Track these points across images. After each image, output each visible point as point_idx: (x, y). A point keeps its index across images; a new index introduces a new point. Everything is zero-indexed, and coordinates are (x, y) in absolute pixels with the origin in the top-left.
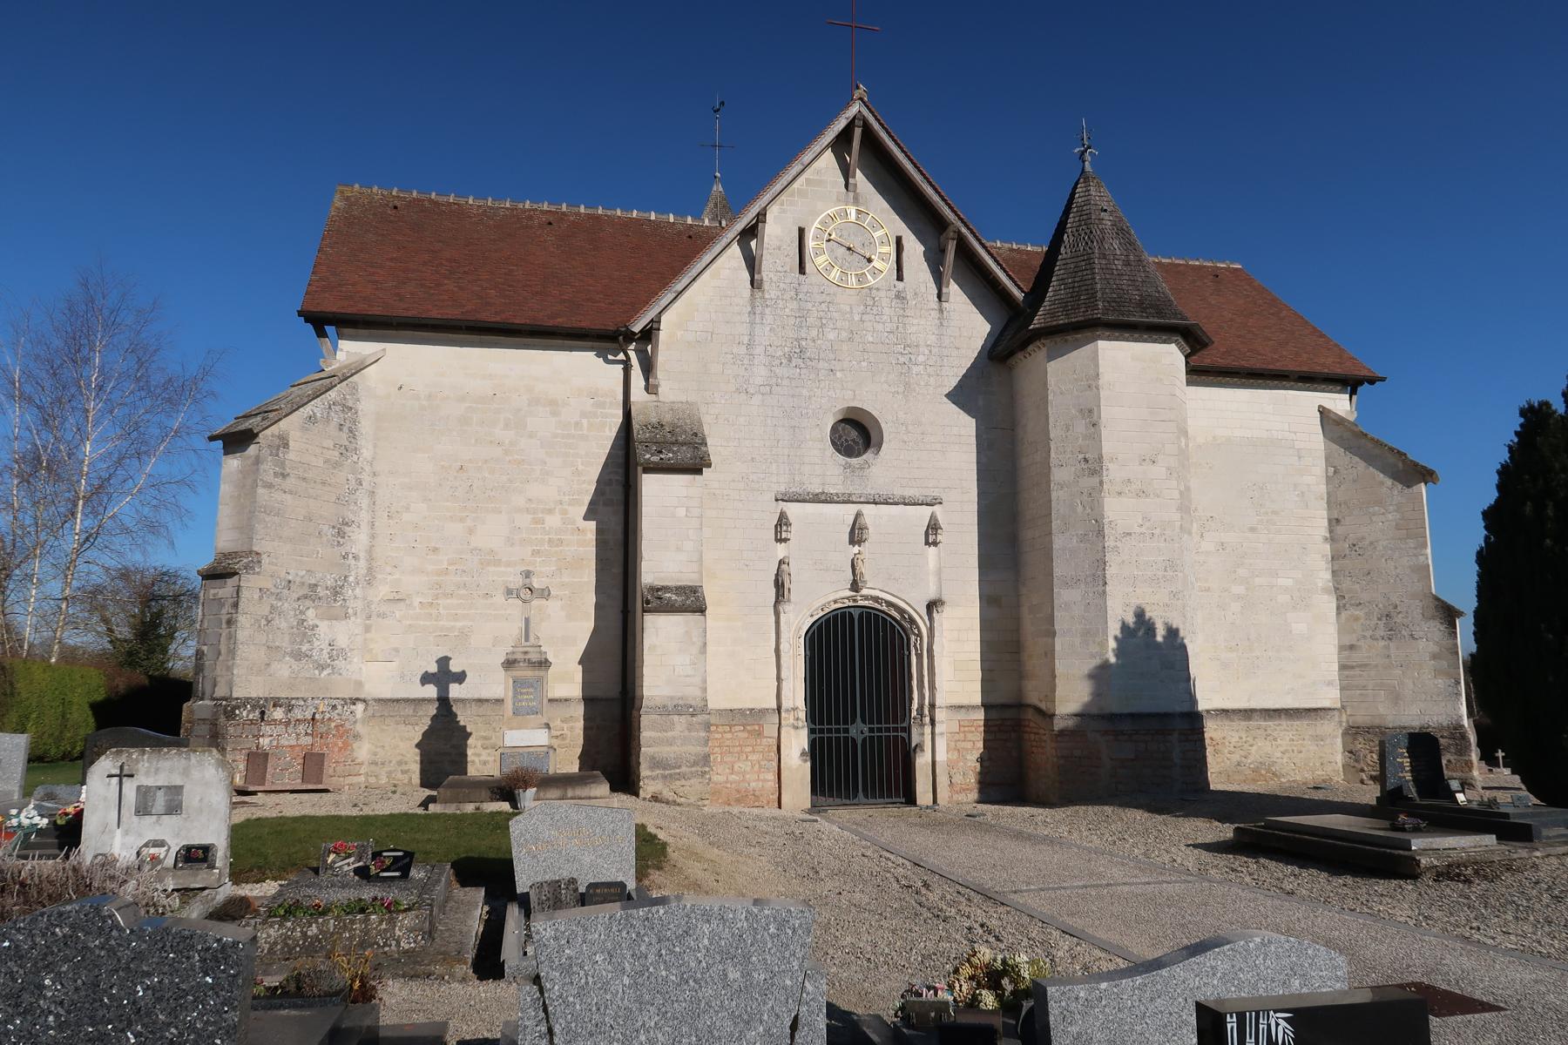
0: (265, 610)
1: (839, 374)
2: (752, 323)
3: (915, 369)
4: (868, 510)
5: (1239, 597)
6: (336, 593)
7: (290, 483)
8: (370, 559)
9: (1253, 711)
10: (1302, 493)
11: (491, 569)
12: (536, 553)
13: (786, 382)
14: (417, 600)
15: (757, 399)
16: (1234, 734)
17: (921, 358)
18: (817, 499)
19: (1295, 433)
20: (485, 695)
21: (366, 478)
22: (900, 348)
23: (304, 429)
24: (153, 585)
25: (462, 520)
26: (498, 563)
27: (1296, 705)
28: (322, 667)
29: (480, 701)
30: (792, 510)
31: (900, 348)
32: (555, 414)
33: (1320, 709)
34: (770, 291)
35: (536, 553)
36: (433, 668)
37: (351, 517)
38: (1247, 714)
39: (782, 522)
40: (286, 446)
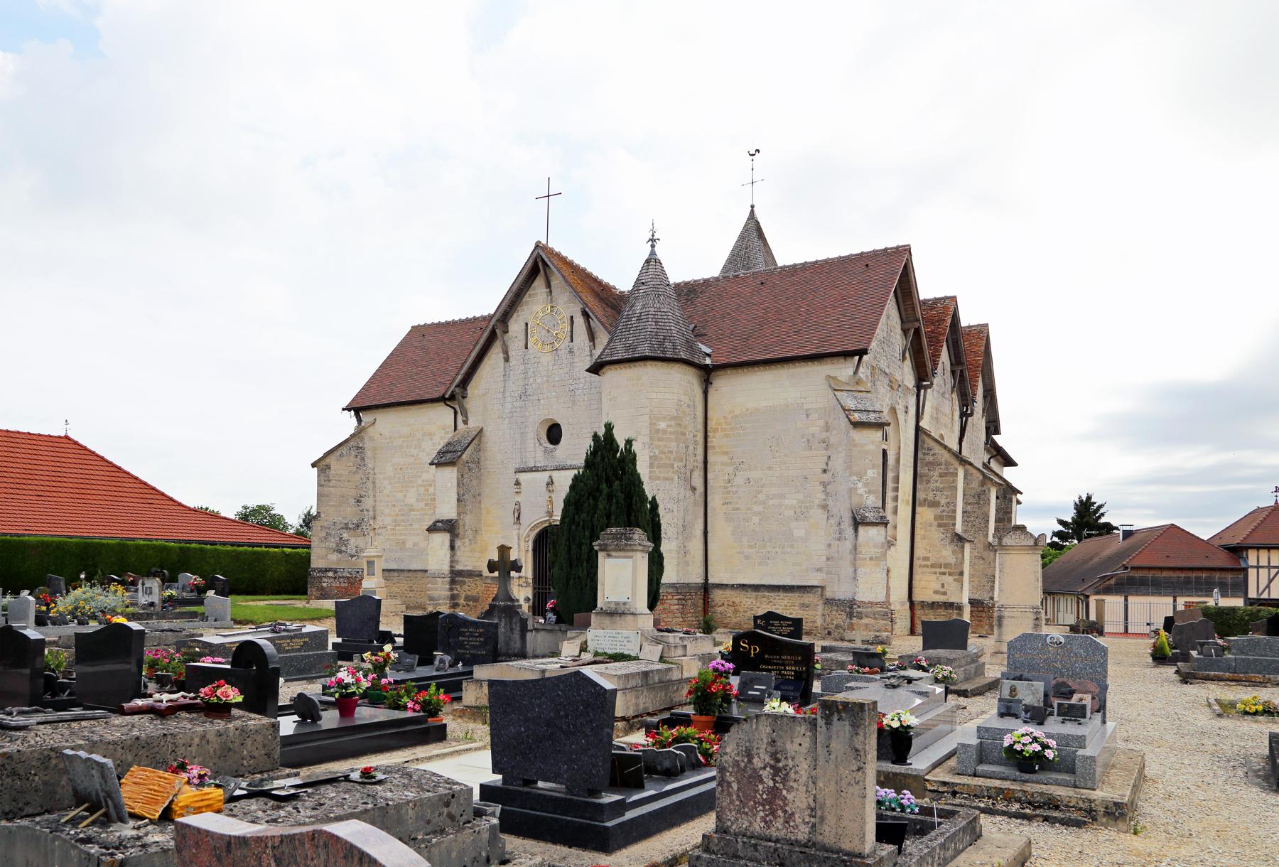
0: (324, 534)
1: (542, 401)
2: (504, 381)
3: (578, 392)
4: (555, 474)
5: (759, 513)
6: (358, 526)
7: (332, 483)
8: (374, 511)
9: (746, 585)
10: (808, 440)
11: (412, 513)
12: (427, 504)
13: (519, 410)
14: (389, 527)
15: (506, 421)
16: (747, 600)
17: (581, 385)
18: (531, 470)
19: (805, 398)
20: (411, 568)
21: (371, 476)
22: (571, 381)
23: (337, 460)
24: (639, 496)
25: (402, 492)
26: (414, 510)
27: (794, 583)
28: (352, 556)
29: (409, 571)
30: (523, 477)
31: (571, 381)
32: (431, 439)
33: (809, 586)
34: (513, 361)
35: (427, 504)
36: (495, 557)
37: (364, 493)
38: (756, 588)
39: (518, 483)
40: (330, 468)
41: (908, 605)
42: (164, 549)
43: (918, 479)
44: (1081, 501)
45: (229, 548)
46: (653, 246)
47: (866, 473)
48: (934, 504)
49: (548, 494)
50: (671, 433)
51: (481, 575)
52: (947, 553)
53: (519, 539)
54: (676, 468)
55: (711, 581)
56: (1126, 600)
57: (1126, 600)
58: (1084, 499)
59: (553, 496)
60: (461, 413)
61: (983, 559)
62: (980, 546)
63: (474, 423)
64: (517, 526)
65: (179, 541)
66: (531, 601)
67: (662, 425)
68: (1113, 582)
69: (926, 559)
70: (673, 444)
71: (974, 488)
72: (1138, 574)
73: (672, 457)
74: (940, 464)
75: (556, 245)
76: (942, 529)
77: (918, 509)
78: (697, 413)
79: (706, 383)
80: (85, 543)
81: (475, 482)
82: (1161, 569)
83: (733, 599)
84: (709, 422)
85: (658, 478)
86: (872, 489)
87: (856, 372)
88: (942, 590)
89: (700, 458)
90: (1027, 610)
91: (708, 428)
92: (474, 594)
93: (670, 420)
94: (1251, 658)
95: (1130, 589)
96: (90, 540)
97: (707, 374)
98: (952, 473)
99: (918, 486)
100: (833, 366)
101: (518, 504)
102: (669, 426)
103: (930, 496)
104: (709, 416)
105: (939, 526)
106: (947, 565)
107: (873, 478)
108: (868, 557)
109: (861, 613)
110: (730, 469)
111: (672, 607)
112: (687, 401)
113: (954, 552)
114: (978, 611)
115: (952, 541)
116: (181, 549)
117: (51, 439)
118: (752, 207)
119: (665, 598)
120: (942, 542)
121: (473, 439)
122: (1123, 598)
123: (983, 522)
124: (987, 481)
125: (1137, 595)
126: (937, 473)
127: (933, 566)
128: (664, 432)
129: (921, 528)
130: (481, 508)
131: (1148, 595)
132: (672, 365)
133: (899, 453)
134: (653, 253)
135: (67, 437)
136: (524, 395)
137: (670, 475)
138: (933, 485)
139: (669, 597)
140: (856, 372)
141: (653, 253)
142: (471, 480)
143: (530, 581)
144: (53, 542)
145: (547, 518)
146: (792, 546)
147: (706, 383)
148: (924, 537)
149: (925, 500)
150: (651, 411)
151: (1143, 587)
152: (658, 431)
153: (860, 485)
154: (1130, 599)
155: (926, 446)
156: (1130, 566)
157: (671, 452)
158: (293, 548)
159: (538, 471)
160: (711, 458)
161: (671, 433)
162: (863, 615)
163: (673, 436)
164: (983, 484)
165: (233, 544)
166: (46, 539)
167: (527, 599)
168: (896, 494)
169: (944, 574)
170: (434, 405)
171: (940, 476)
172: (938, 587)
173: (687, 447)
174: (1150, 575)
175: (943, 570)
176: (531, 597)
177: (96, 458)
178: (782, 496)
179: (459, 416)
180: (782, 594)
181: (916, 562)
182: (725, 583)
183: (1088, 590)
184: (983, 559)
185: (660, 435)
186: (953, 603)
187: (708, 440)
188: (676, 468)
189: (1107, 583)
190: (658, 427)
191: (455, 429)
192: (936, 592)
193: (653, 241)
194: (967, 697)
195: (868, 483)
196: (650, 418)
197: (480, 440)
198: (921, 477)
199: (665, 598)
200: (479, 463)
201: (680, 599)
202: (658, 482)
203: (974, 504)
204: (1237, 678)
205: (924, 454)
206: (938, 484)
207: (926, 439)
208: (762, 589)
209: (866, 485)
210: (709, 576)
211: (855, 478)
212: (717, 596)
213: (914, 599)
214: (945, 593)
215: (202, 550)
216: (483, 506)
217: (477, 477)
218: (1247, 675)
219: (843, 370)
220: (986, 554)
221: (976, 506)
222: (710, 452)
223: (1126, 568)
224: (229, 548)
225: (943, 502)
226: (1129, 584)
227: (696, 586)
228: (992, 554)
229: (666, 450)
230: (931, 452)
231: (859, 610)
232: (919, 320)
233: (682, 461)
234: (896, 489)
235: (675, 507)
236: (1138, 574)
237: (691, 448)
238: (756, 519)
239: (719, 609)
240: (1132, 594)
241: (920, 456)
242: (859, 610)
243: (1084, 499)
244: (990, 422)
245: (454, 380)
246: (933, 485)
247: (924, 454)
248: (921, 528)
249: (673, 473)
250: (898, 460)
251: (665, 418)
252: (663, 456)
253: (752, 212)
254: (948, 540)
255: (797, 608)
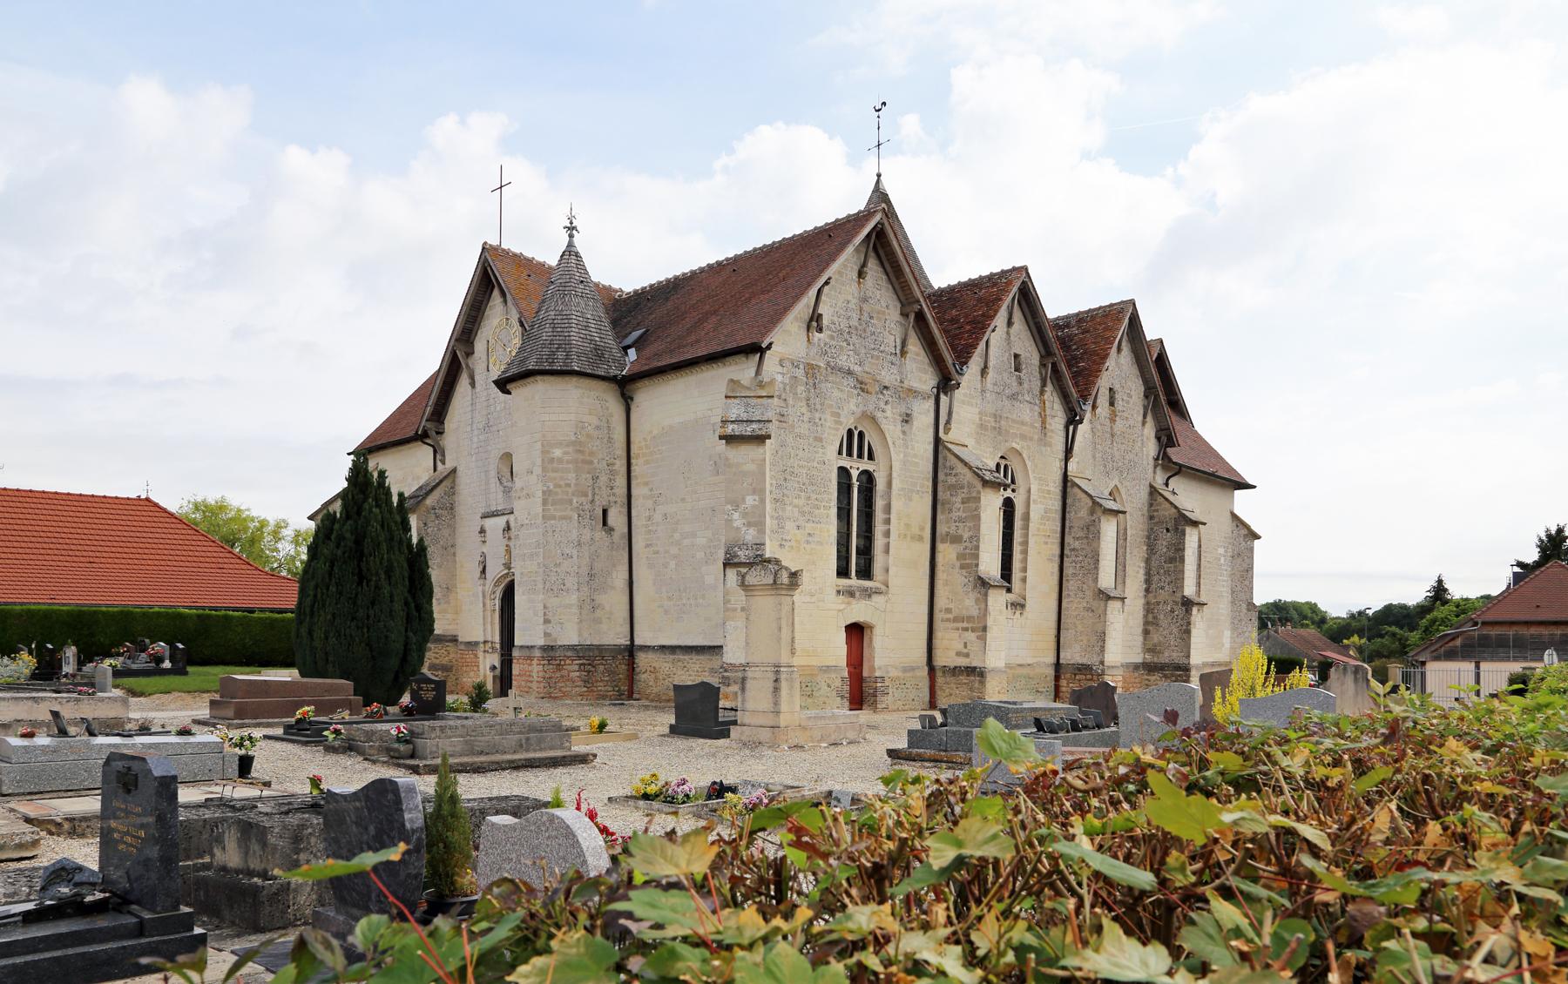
19: (711, 410)
38: (673, 649)
39: (482, 531)
41: (924, 672)
42: (180, 615)
43: (939, 507)
44: (1549, 536)
45: (268, 614)
46: (571, 236)
47: (744, 500)
48: (956, 539)
49: (505, 542)
50: (568, 462)
51: (456, 641)
52: (969, 604)
53: (484, 596)
54: (575, 504)
55: (638, 642)
56: (1478, 667)
57: (1478, 667)
58: (1553, 532)
59: (511, 544)
60: (438, 452)
61: (1093, 611)
62: (1089, 593)
63: (449, 464)
64: (482, 581)
65: (197, 608)
66: (499, 670)
67: (557, 453)
68: (1458, 642)
69: (948, 611)
70: (572, 476)
71: (1081, 518)
72: (1494, 632)
73: (570, 491)
74: (962, 487)
75: (512, 244)
76: (964, 571)
77: (940, 547)
78: (615, 436)
79: (627, 400)
80: (80, 611)
81: (446, 532)
82: (1527, 623)
83: (654, 665)
84: (632, 446)
85: (554, 518)
86: (752, 520)
87: (758, 372)
88: (965, 651)
89: (623, 491)
90: (768, 669)
91: (632, 454)
92: (444, 662)
93: (567, 446)
94: (962, 730)
95: (1484, 652)
96: (10, 607)
97: (625, 386)
98: (975, 498)
99: (940, 517)
100: (737, 367)
101: (483, 555)
102: (566, 453)
103: (952, 531)
104: (632, 439)
105: (962, 567)
106: (970, 619)
107: (753, 506)
108: (739, 607)
109: (728, 678)
110: (649, 503)
111: (573, 674)
112: (595, 421)
113: (977, 600)
114: (1086, 679)
115: (975, 587)
116: (199, 616)
117: (70, 498)
118: (879, 176)
119: (562, 663)
120: (965, 589)
121: (441, 481)
122: (1473, 665)
123: (1092, 561)
124: (1097, 508)
125: (1492, 661)
126: (959, 499)
127: (955, 620)
128: (560, 461)
129: (943, 571)
130: (455, 561)
131: (1509, 661)
132: (567, 378)
133: (891, 475)
134: (570, 245)
135: (147, 499)
136: (487, 427)
137: (569, 513)
138: (955, 515)
139: (568, 662)
140: (758, 372)
141: (570, 245)
142: (439, 530)
143: (498, 646)
144: (39, 610)
145: (506, 571)
146: (703, 597)
147: (627, 400)
148: (946, 583)
149: (948, 534)
150: (544, 436)
151: (1501, 650)
152: (552, 460)
153: (736, 516)
154: (1483, 666)
155: (948, 464)
156: (1480, 621)
157: (568, 485)
158: (216, 610)
159: (498, 515)
160: (634, 492)
161: (568, 462)
162: (731, 681)
163: (570, 466)
164: (1092, 512)
165: (272, 611)
166: (33, 607)
167: (493, 668)
168: (887, 527)
169: (966, 629)
170: (400, 448)
171: (963, 503)
172: (960, 647)
173: (595, 479)
174: (1511, 632)
175: (965, 625)
176: (497, 664)
177: (174, 520)
178: (694, 535)
179: (438, 457)
180: (695, 657)
181: (938, 616)
182: (648, 644)
183: (1423, 653)
184: (1093, 611)
185: (555, 465)
186: (975, 668)
187: (632, 468)
188: (575, 504)
189: (1451, 644)
190: (552, 456)
191: (435, 470)
192: (959, 654)
193: (571, 229)
194: (419, 774)
195: (746, 514)
196: (543, 445)
197: (454, 481)
198: (943, 504)
199: (562, 663)
200: (452, 509)
201: (581, 664)
202: (552, 522)
203: (1082, 538)
204: (939, 758)
205: (946, 475)
206: (960, 514)
207: (948, 455)
208: (678, 651)
209: (745, 515)
210: (635, 636)
211: (729, 507)
212: (642, 659)
213: (935, 663)
214: (967, 655)
215: (226, 617)
216: (457, 559)
217: (449, 526)
218: (949, 754)
219: (743, 370)
220: (1095, 604)
221: (1085, 541)
222: (634, 483)
223: (1476, 624)
224: (268, 614)
225: (966, 536)
226: (1480, 645)
227: (616, 650)
228: (1102, 603)
229: (562, 483)
230: (954, 472)
231: (725, 674)
232: (918, 301)
233: (587, 496)
234: (888, 521)
235: (575, 552)
236: (1494, 632)
237: (603, 479)
238: (672, 564)
239: (643, 676)
240: (1485, 660)
241: (941, 476)
242: (725, 674)
243: (1553, 531)
244: (1162, 430)
245: (424, 413)
246: (955, 515)
247: (946, 475)
248: (943, 571)
249: (572, 510)
250: (889, 484)
251: (561, 444)
252: (558, 490)
253: (878, 182)
254: (971, 586)
255: (707, 674)
